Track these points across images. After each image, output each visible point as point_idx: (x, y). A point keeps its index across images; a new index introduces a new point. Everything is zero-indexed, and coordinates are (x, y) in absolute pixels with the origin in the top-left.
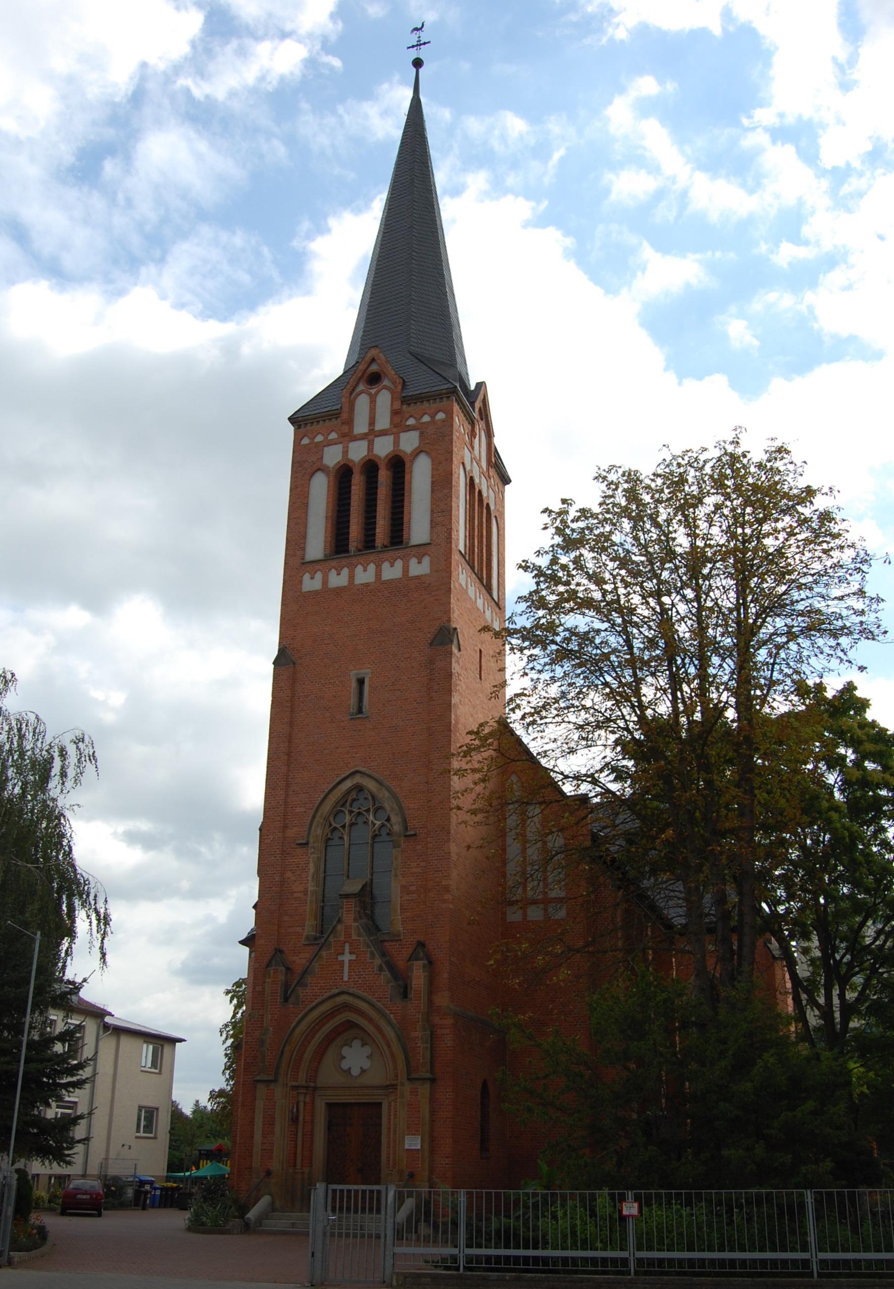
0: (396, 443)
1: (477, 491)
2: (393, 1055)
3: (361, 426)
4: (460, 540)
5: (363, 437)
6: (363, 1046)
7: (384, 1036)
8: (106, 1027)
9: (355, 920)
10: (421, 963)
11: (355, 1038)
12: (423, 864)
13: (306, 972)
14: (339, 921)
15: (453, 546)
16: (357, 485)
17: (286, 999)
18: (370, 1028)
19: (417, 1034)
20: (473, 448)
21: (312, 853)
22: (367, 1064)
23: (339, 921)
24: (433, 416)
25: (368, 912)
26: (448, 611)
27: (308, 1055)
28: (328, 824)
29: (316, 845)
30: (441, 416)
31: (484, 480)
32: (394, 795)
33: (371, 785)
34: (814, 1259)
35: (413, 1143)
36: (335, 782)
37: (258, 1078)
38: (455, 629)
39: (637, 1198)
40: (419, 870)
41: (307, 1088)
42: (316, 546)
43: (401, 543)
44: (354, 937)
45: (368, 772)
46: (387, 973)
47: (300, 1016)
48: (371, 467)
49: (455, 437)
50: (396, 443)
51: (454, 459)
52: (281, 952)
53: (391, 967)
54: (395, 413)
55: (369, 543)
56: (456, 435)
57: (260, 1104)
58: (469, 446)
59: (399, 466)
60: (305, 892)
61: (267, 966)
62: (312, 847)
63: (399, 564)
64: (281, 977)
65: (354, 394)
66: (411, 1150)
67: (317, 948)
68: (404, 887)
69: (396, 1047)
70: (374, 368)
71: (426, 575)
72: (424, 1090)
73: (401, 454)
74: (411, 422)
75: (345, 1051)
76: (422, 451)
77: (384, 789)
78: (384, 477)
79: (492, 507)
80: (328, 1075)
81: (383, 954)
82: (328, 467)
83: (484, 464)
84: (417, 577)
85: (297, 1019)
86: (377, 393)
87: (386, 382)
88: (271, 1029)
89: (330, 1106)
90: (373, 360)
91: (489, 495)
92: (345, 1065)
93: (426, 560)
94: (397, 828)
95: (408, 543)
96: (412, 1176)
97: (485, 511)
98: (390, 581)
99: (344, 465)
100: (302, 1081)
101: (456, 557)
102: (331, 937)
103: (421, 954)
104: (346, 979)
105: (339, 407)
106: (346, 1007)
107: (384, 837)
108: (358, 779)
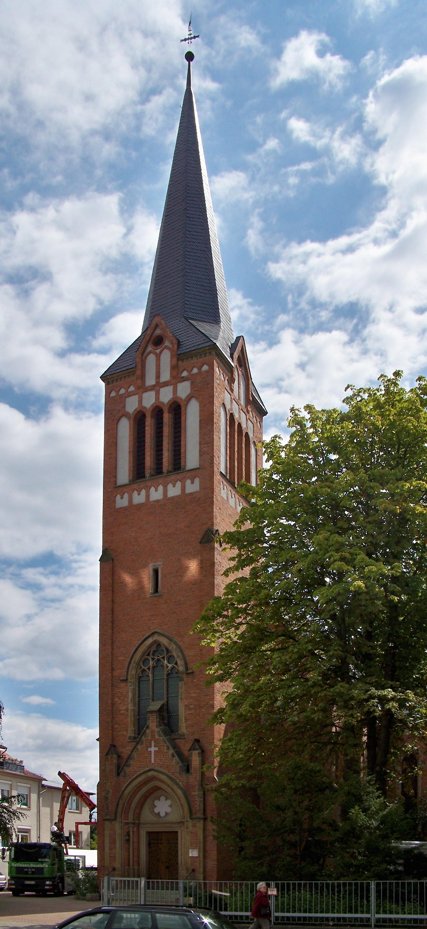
0: (175, 391)
1: (237, 424)
2: (182, 805)
3: (150, 381)
4: (221, 463)
5: (152, 388)
6: (166, 800)
7: (176, 794)
8: (43, 786)
9: (157, 727)
10: (196, 752)
11: (162, 795)
12: (198, 691)
13: (129, 757)
14: (148, 727)
15: (215, 469)
16: (149, 422)
17: (118, 774)
18: (169, 790)
19: (196, 793)
20: (232, 390)
21: (130, 686)
22: (169, 810)
23: (148, 727)
24: (200, 369)
25: (166, 721)
26: (211, 518)
27: (134, 805)
28: (139, 668)
29: (132, 680)
30: (205, 368)
31: (243, 414)
32: (179, 647)
33: (164, 641)
34: (373, 918)
35: (194, 853)
36: (142, 640)
37: (104, 818)
38: (217, 530)
39: (277, 886)
40: (195, 695)
41: (134, 823)
42: (124, 475)
43: (179, 468)
44: (157, 737)
45: (162, 632)
46: (177, 758)
47: (127, 783)
48: (158, 411)
49: (215, 385)
50: (175, 391)
51: (215, 402)
52: (114, 746)
53: (180, 754)
54: (174, 368)
55: (158, 470)
56: (216, 382)
57: (107, 832)
58: (228, 389)
59: (177, 409)
60: (127, 710)
61: (106, 755)
62: (130, 682)
63: (179, 484)
64: (115, 761)
65: (145, 354)
66: (193, 857)
67: (135, 743)
68: (187, 706)
69: (183, 801)
70: (158, 332)
71: (196, 492)
72: (200, 824)
73: (178, 400)
74: (185, 374)
75: (156, 802)
76: (192, 397)
77: (173, 644)
78: (167, 417)
79: (251, 435)
80: (146, 816)
81: (175, 747)
82: (129, 413)
83: (242, 402)
84: (191, 494)
85: (125, 785)
86: (161, 352)
87: (167, 343)
88: (111, 791)
89: (149, 833)
90: (157, 326)
91: (248, 426)
92: (156, 810)
93: (197, 481)
94: (181, 668)
95: (184, 468)
96: (193, 870)
97: (244, 439)
98: (173, 498)
99: (140, 411)
100: (131, 820)
101: (217, 477)
102: (143, 737)
103: (197, 747)
104: (153, 761)
105: (134, 365)
106: (153, 778)
107: (174, 675)
108: (156, 637)
